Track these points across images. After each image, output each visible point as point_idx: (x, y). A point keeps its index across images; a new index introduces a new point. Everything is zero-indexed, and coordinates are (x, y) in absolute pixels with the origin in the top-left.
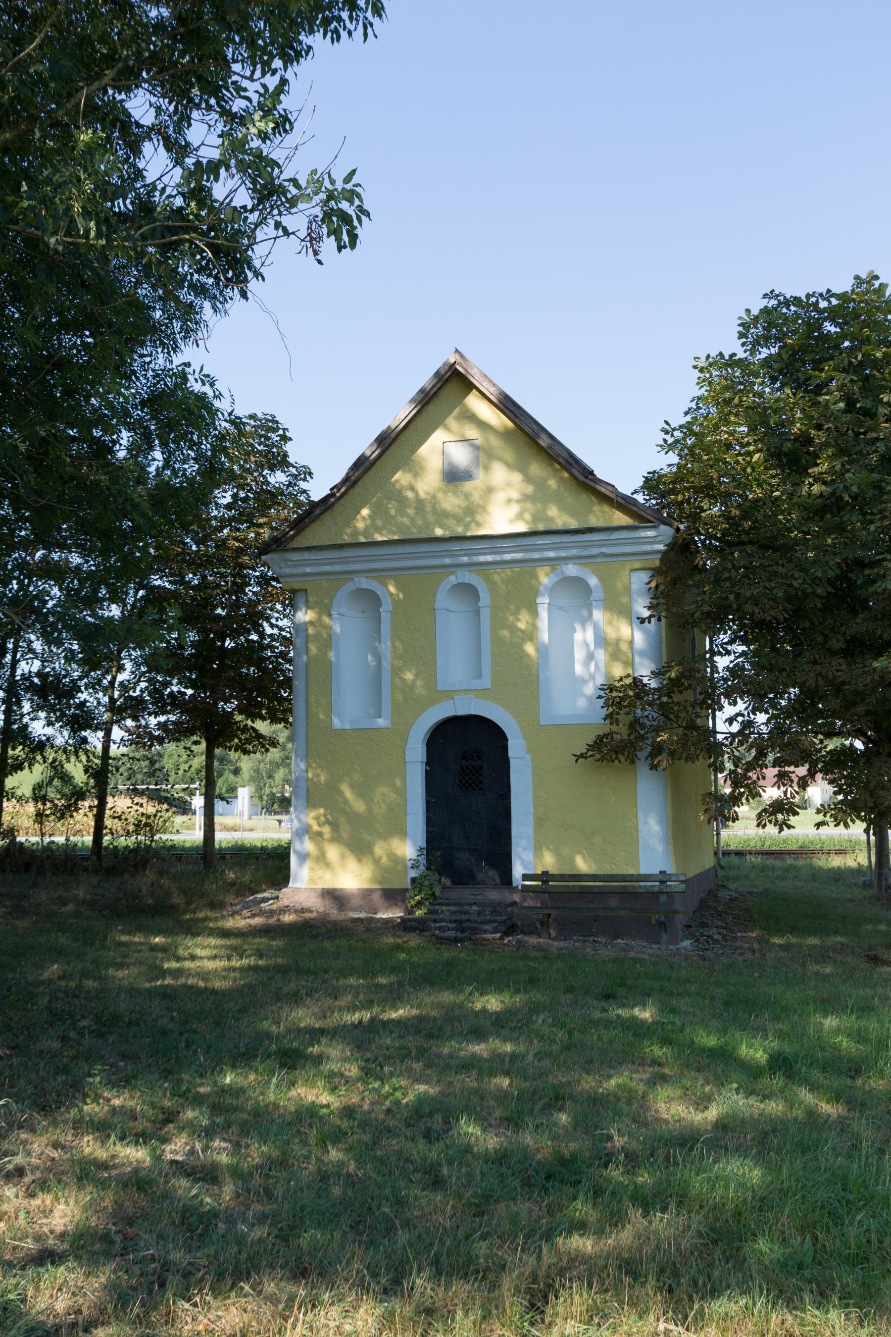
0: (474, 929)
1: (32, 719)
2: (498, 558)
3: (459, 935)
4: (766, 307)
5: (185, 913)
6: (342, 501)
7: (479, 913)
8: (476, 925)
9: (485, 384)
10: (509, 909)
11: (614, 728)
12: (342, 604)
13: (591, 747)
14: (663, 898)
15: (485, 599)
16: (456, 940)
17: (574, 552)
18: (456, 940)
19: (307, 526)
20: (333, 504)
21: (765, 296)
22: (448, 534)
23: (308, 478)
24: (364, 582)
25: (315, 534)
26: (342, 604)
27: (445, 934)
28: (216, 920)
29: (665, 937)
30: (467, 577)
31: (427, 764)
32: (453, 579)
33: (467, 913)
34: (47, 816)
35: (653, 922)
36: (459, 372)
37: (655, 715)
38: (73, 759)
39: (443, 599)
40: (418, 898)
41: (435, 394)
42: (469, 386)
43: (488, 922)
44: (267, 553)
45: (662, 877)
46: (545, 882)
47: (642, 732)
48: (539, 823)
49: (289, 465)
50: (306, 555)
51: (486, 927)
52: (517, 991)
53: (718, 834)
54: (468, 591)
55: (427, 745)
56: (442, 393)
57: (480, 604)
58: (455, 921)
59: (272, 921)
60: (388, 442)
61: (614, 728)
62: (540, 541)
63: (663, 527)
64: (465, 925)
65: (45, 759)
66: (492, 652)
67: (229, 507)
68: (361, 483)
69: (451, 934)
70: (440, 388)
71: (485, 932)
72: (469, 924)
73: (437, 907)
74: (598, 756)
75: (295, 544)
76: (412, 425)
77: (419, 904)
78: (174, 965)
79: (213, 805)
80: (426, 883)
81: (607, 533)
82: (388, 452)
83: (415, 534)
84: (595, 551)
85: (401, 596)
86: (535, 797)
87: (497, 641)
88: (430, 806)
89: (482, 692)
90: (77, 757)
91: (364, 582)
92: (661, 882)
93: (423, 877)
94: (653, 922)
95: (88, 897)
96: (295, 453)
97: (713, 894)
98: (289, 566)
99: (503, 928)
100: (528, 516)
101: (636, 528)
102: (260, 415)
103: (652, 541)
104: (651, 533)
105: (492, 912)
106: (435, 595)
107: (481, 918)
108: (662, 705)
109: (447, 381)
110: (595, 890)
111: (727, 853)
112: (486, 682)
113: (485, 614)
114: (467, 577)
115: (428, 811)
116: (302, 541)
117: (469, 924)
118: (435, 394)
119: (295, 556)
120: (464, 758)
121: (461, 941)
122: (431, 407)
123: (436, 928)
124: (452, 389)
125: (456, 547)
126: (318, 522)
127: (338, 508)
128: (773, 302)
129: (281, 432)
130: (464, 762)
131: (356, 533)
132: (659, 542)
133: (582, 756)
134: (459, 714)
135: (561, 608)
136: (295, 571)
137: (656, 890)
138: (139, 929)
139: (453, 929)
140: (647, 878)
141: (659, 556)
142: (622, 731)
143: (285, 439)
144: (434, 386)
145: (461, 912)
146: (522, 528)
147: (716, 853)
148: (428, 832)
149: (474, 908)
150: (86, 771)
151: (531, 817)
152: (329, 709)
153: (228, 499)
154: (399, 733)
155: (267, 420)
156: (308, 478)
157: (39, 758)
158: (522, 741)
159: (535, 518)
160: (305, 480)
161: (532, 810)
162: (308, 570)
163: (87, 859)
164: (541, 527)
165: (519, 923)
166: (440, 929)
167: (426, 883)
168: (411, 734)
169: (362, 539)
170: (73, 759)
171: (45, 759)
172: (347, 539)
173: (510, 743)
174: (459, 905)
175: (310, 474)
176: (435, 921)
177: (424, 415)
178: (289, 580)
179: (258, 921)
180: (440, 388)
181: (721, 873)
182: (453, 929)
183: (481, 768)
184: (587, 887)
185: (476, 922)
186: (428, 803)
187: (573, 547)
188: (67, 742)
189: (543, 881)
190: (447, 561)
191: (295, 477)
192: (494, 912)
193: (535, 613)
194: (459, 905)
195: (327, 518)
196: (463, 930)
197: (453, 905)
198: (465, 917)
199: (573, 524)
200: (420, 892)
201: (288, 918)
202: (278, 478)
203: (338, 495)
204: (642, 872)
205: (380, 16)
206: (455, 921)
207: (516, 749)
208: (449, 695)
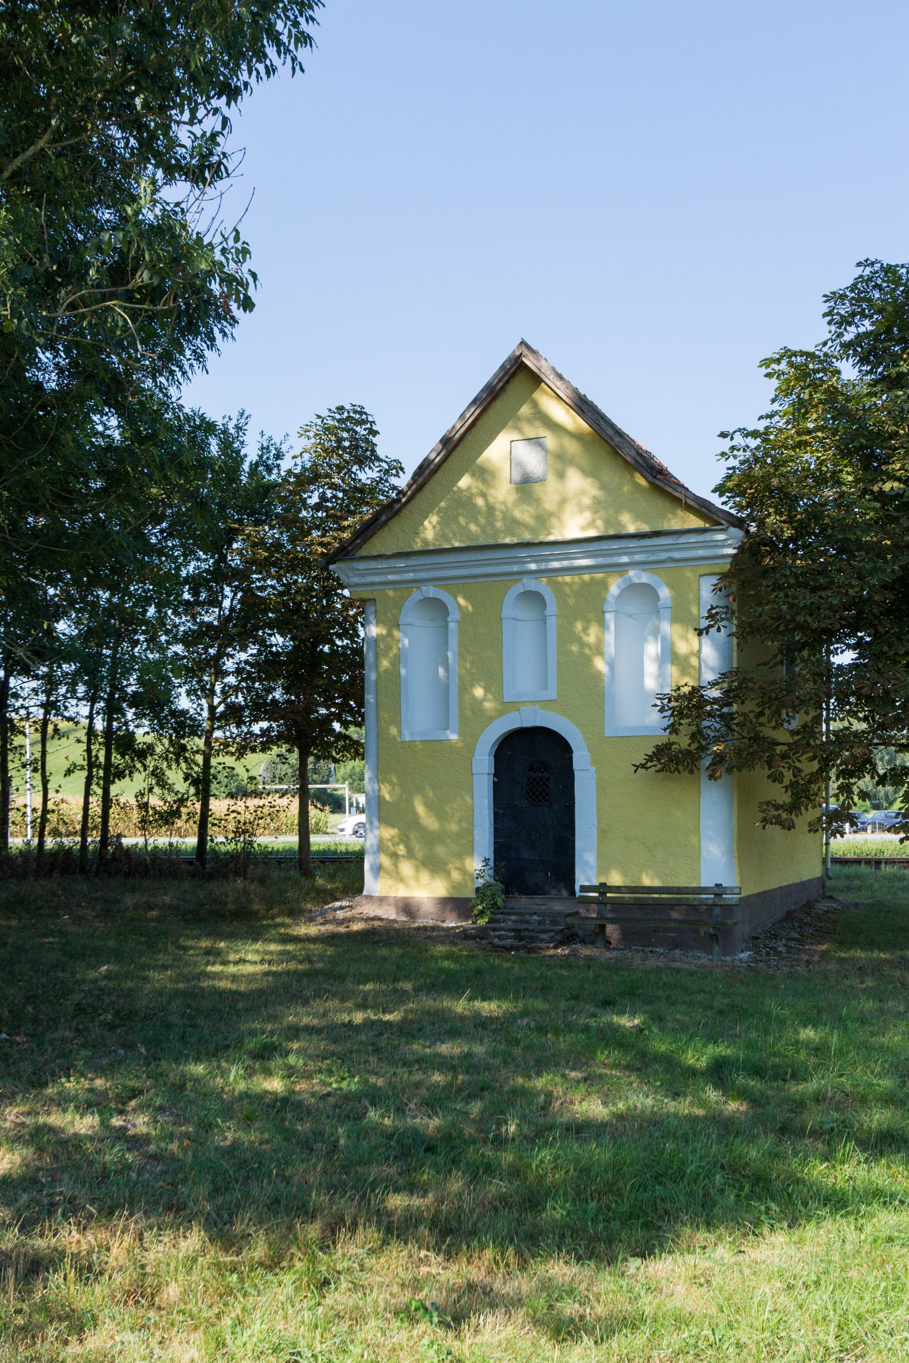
0: (531, 938)
1: (137, 727)
2: (566, 563)
3: (516, 943)
4: (861, 276)
5: (264, 918)
6: (409, 506)
7: (539, 923)
8: (533, 934)
9: (551, 377)
10: (569, 920)
11: (674, 738)
12: (411, 615)
13: (650, 758)
14: (717, 911)
15: (552, 608)
16: (511, 948)
17: (638, 558)
18: (511, 948)
19: (374, 533)
20: (400, 510)
21: (859, 264)
22: (515, 540)
23: (401, 473)
24: (431, 591)
25: (383, 542)
26: (411, 615)
27: (502, 943)
28: (287, 926)
29: (717, 948)
30: (530, 584)
31: (495, 775)
32: (519, 588)
33: (527, 922)
34: (151, 822)
35: (702, 934)
36: (526, 367)
37: (718, 726)
38: (174, 766)
39: (510, 608)
40: (480, 907)
41: (502, 388)
42: (536, 380)
43: (545, 931)
44: (334, 563)
45: (717, 890)
46: (603, 894)
47: (704, 743)
48: (603, 834)
49: (379, 459)
50: (373, 564)
51: (544, 936)
52: (516, 998)
53: (827, 844)
54: (535, 598)
55: (495, 756)
56: (511, 388)
57: (547, 613)
58: (513, 930)
59: (342, 929)
60: (451, 446)
61: (674, 738)
62: (615, 545)
63: (733, 530)
64: (523, 934)
65: (145, 767)
66: (559, 663)
67: (318, 507)
68: (428, 488)
69: (509, 942)
70: (507, 382)
71: (542, 941)
72: (526, 933)
73: (499, 916)
74: (659, 766)
75: (363, 552)
76: (479, 424)
77: (482, 913)
78: (217, 968)
79: (307, 812)
80: (488, 893)
81: (674, 537)
82: (455, 454)
83: (482, 541)
84: (663, 556)
85: (470, 608)
86: (599, 810)
87: (563, 652)
88: (498, 818)
89: (547, 704)
90: (178, 764)
91: (431, 591)
92: (716, 894)
93: (487, 886)
94: (702, 934)
95: (175, 903)
96: (384, 447)
97: (809, 906)
98: (356, 575)
99: (559, 937)
100: (599, 523)
101: (704, 531)
102: (348, 407)
103: (722, 544)
104: (721, 537)
105: (551, 922)
106: (501, 604)
107: (539, 928)
108: (722, 716)
109: (513, 375)
110: (650, 902)
111: (836, 861)
112: (552, 693)
113: (552, 622)
114: (530, 584)
115: (495, 822)
116: (370, 548)
117: (526, 933)
118: (502, 388)
119: (362, 565)
120: (531, 769)
121: (516, 949)
122: (498, 404)
123: (495, 937)
124: (518, 385)
125: (523, 553)
126: (386, 529)
127: (405, 512)
128: (868, 270)
129: (368, 426)
130: (531, 774)
131: (425, 541)
132: (729, 546)
133: (643, 766)
134: (525, 725)
135: (630, 616)
136: (363, 580)
137: (710, 902)
138: (208, 935)
139: (511, 938)
140: (704, 890)
141: (729, 560)
142: (683, 741)
143: (375, 433)
144: (500, 381)
145: (522, 922)
146: (592, 533)
147: (824, 861)
148: (495, 843)
149: (535, 917)
150: (186, 779)
151: (595, 829)
152: (398, 724)
153: (314, 499)
154: (470, 748)
155: (355, 412)
156: (401, 473)
157: (139, 765)
158: (587, 753)
159: (607, 523)
160: (397, 475)
161: (595, 822)
162: (377, 579)
163: (190, 863)
164: (611, 532)
165: (580, 932)
166: (499, 937)
167: (488, 893)
168: (478, 746)
169: (527, 537)
170: (174, 766)
171: (145, 767)
172: (418, 546)
173: (575, 756)
174: (519, 914)
175: (402, 469)
176: (495, 930)
177: (491, 412)
178: (358, 589)
179: (330, 928)
180: (507, 382)
181: (829, 883)
182: (511, 938)
183: (548, 780)
184: (643, 899)
185: (533, 931)
186: (497, 817)
187: (638, 553)
188: (168, 751)
189: (600, 893)
190: (515, 568)
191: (387, 472)
192: (554, 922)
193: (602, 624)
194: (519, 914)
195: (394, 524)
196: (521, 939)
197: (515, 914)
198: (525, 926)
199: (645, 528)
200: (482, 902)
201: (356, 927)
202: (367, 475)
203: (404, 500)
204: (703, 885)
205: (269, 77)
206: (513, 930)
207: (581, 760)
208: (514, 706)
